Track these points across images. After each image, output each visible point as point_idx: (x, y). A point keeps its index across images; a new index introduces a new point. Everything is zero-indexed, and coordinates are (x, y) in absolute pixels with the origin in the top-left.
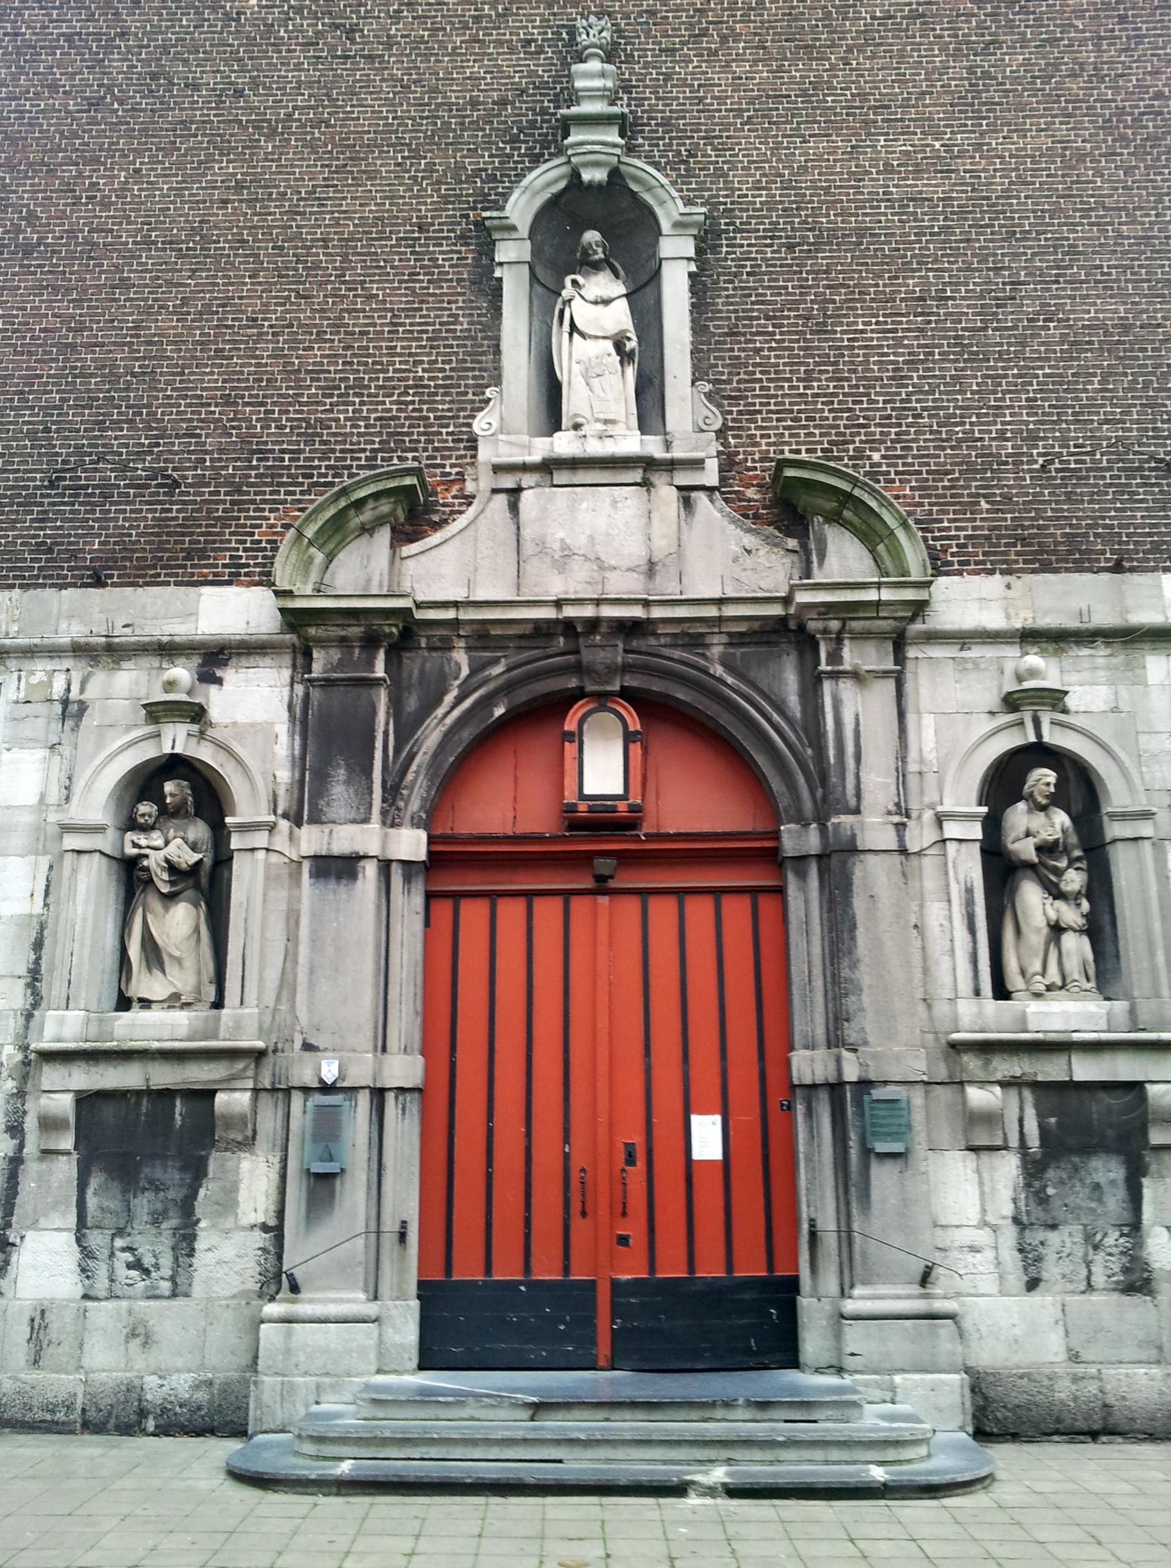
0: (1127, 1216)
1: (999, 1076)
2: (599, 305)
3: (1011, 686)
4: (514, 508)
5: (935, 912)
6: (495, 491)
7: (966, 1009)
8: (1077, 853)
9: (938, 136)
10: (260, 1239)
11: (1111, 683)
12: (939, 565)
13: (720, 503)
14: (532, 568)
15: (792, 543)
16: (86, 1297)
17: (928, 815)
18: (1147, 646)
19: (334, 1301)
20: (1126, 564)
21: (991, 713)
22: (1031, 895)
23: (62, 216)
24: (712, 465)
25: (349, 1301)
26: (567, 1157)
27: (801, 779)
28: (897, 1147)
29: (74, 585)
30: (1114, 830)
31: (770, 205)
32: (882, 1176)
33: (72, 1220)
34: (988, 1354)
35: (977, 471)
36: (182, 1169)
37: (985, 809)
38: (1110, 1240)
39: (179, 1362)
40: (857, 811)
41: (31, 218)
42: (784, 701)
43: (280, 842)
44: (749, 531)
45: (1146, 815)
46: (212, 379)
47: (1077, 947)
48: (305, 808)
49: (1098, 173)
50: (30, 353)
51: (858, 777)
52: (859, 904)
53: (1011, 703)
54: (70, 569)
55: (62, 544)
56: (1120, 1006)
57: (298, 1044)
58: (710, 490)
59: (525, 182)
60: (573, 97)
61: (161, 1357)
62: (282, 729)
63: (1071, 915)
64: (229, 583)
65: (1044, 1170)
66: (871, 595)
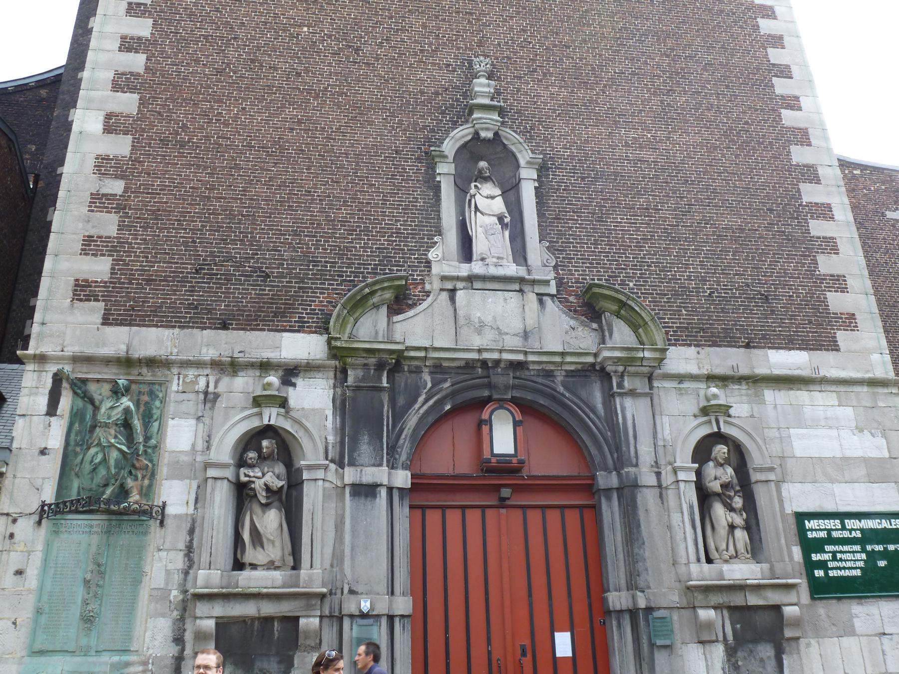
1: (712, 604)
3: (703, 403)
4: (452, 299)
5: (676, 518)
6: (442, 290)
7: (694, 568)
8: (738, 488)
9: (649, 131)
11: (749, 403)
13: (557, 303)
14: (464, 331)
15: (595, 326)
17: (669, 468)
18: (764, 385)
20: (752, 344)
21: (695, 416)
23: (202, 128)
24: (553, 283)
26: (489, 653)
28: (668, 642)
29: (210, 328)
30: (755, 476)
31: (572, 157)
32: (660, 658)
36: (280, 662)
40: (637, 465)
41: (184, 127)
42: (595, 407)
43: (331, 476)
44: (572, 318)
45: (772, 469)
46: (287, 221)
47: (741, 535)
50: (184, 200)
51: (636, 447)
53: (705, 411)
54: (208, 319)
55: (203, 305)
58: (552, 296)
59: (452, 134)
62: (329, 413)
63: (738, 520)
64: (298, 331)
66: (641, 355)
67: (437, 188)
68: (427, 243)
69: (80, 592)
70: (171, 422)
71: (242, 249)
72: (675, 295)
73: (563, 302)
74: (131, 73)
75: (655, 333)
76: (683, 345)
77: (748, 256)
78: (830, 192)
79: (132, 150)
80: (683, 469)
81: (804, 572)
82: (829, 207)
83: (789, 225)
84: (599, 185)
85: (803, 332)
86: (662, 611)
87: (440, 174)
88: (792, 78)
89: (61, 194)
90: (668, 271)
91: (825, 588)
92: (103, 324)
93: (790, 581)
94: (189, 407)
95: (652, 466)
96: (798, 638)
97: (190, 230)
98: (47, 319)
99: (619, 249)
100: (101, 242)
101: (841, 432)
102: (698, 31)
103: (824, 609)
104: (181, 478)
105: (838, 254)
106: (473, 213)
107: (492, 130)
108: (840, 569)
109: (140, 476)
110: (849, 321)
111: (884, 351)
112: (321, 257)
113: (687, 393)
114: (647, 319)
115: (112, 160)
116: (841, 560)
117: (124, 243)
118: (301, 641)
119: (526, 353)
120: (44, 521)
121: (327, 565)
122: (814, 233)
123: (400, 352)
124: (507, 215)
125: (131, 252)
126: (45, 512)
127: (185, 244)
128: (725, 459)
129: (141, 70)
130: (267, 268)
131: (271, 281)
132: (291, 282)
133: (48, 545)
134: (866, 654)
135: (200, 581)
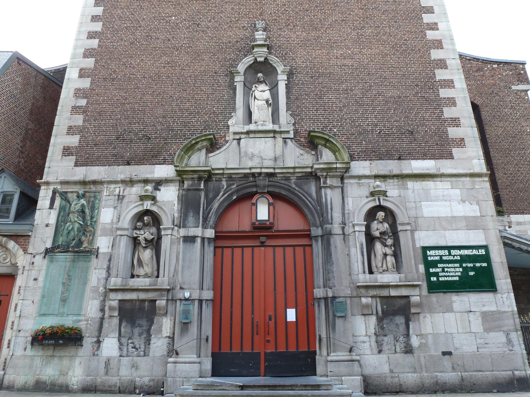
0: (405, 332)
1: (370, 295)
2: (262, 92)
3: (372, 190)
4: (239, 144)
5: (353, 251)
6: (234, 139)
7: (361, 277)
8: (391, 234)
9: (350, 49)
10: (166, 340)
11: (398, 189)
12: (352, 158)
13: (294, 142)
14: (243, 159)
15: (313, 153)
16: (120, 356)
17: (351, 224)
18: (408, 179)
19: (188, 357)
20: (402, 158)
21: (367, 197)
22: (378, 246)
23: (123, 71)
24: (292, 132)
25: (192, 357)
26: (253, 318)
27: (316, 215)
28: (343, 315)
29: (122, 165)
30: (400, 228)
31: (307, 67)
32: (339, 322)
33: (117, 335)
34: (368, 371)
35: (362, 134)
36: (147, 321)
37: (366, 223)
38: (401, 339)
39: (146, 374)
40: (332, 224)
42: (312, 194)
43: (175, 233)
44: (302, 149)
45: (409, 224)
46: (160, 111)
47: (390, 259)
48: (182, 224)
49: (391, 59)
51: (331, 214)
52: (333, 248)
53: (372, 194)
54: (121, 161)
56: (402, 275)
57: (179, 288)
58: (292, 139)
59: (242, 61)
60: (255, 40)
61: (141, 372)
62: (176, 202)
63: (389, 251)
64: (163, 164)
65: (383, 320)
66: (335, 166)
67: (234, 89)
69: (60, 288)
74: (92, 49)
75: (344, 154)
77: (402, 111)
78: (455, 73)
80: (357, 225)
81: (425, 279)
82: (452, 81)
89: (59, 108)
92: (75, 166)
93: (415, 283)
94: (111, 203)
95: (340, 224)
96: (419, 313)
98: (51, 165)
101: (452, 203)
104: (106, 235)
109: (88, 235)
110: (461, 142)
111: (480, 158)
113: (363, 185)
114: (340, 147)
116: (447, 272)
119: (274, 168)
120: (46, 256)
122: (442, 95)
123: (209, 171)
126: (47, 252)
127: (113, 126)
128: (383, 219)
129: (96, 47)
133: (48, 267)
134: (459, 322)
135: (112, 283)
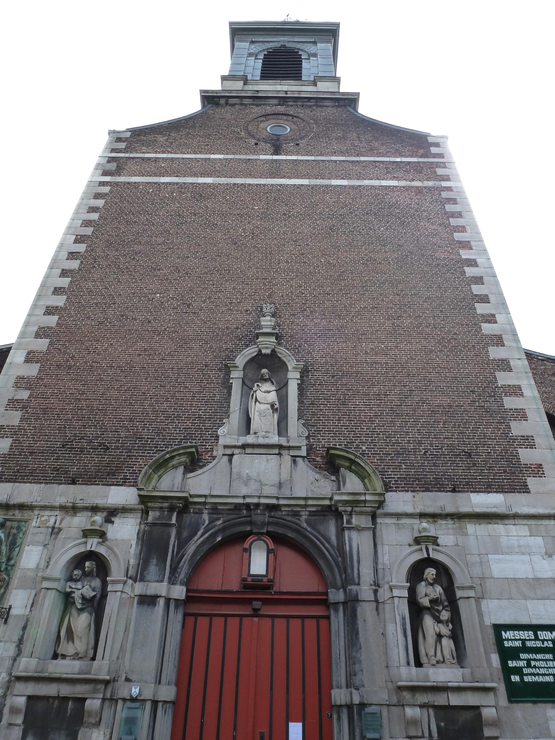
1: (419, 703)
4: (230, 461)
6: (224, 455)
8: (446, 603)
9: (383, 343)
13: (307, 462)
14: (235, 484)
15: (333, 478)
21: (410, 545)
23: (84, 357)
24: (304, 449)
29: (64, 483)
30: (459, 594)
31: (326, 363)
40: (359, 584)
42: (330, 538)
43: (128, 589)
44: (318, 473)
45: (471, 588)
46: (126, 412)
47: (448, 644)
51: (358, 570)
54: (64, 477)
55: (63, 468)
58: (304, 457)
59: (242, 353)
62: (134, 542)
63: (445, 630)
64: (122, 485)
68: (219, 423)
70: (27, 548)
71: (94, 431)
72: (397, 454)
73: (312, 462)
74: (48, 327)
75: (376, 481)
76: (402, 491)
79: (39, 372)
80: (396, 587)
81: (501, 676)
82: (519, 387)
83: (488, 401)
84: (344, 381)
85: (499, 479)
86: (373, 707)
87: (232, 378)
88: (489, 303)
90: (392, 437)
91: (520, 693)
93: (487, 685)
94: (41, 538)
97: (64, 420)
99: (357, 423)
100: (8, 429)
101: (533, 557)
102: (421, 278)
103: (523, 712)
105: (527, 420)
106: (254, 402)
107: (270, 348)
108: (534, 675)
112: (145, 435)
114: (370, 471)
115: (26, 378)
116: (535, 667)
117: (22, 429)
118: (85, 719)
119: (278, 498)
121: (114, 658)
123: (185, 499)
124: (277, 403)
125: (24, 435)
127: (59, 429)
128: (434, 579)
129: (54, 325)
130: (108, 443)
131: (110, 452)
132: (123, 452)
135: (21, 667)
